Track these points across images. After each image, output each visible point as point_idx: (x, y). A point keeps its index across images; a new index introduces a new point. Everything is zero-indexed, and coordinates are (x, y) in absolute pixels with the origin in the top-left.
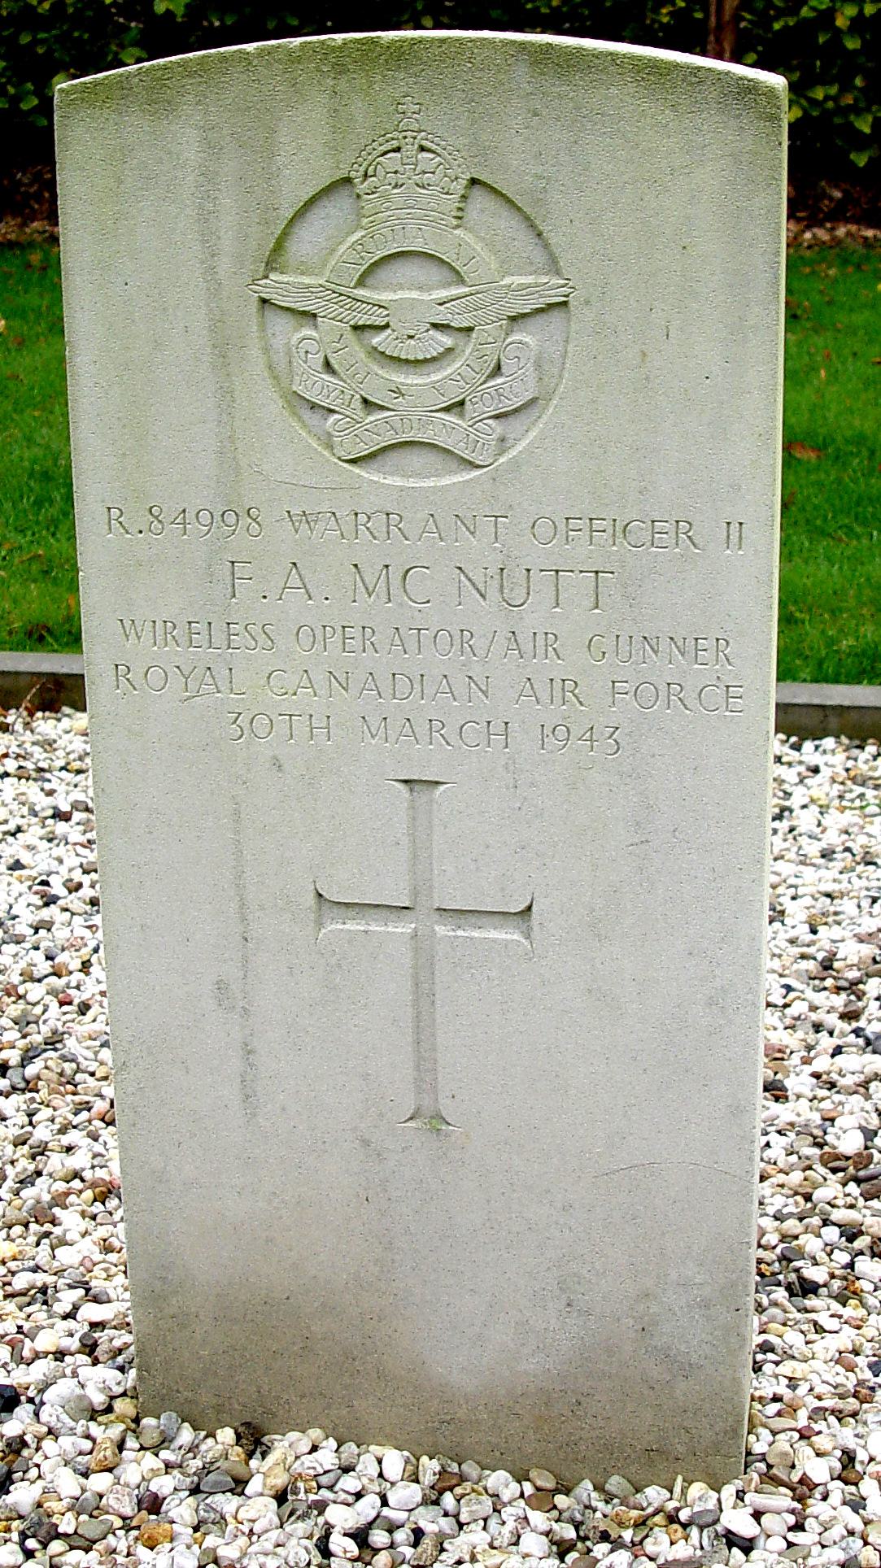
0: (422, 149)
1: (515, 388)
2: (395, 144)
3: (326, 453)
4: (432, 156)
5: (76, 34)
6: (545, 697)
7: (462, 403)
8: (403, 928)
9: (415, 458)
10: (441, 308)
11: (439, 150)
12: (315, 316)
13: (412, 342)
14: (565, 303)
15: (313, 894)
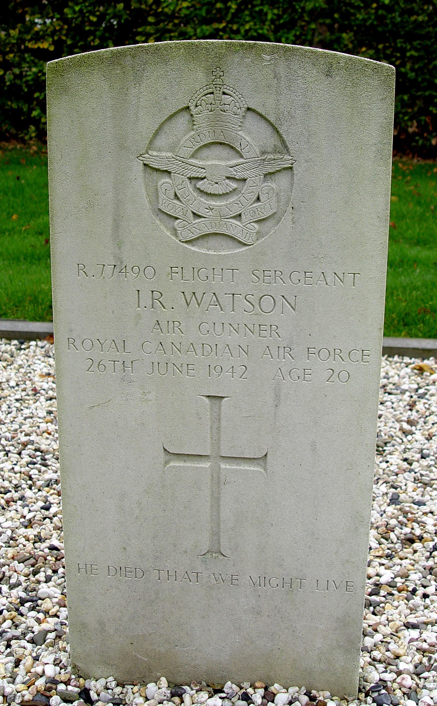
0: (224, 93)
1: (266, 208)
2: (211, 90)
3: (174, 238)
4: (229, 97)
7: (240, 215)
8: (206, 465)
13: (217, 185)
14: (291, 168)
15: (162, 449)
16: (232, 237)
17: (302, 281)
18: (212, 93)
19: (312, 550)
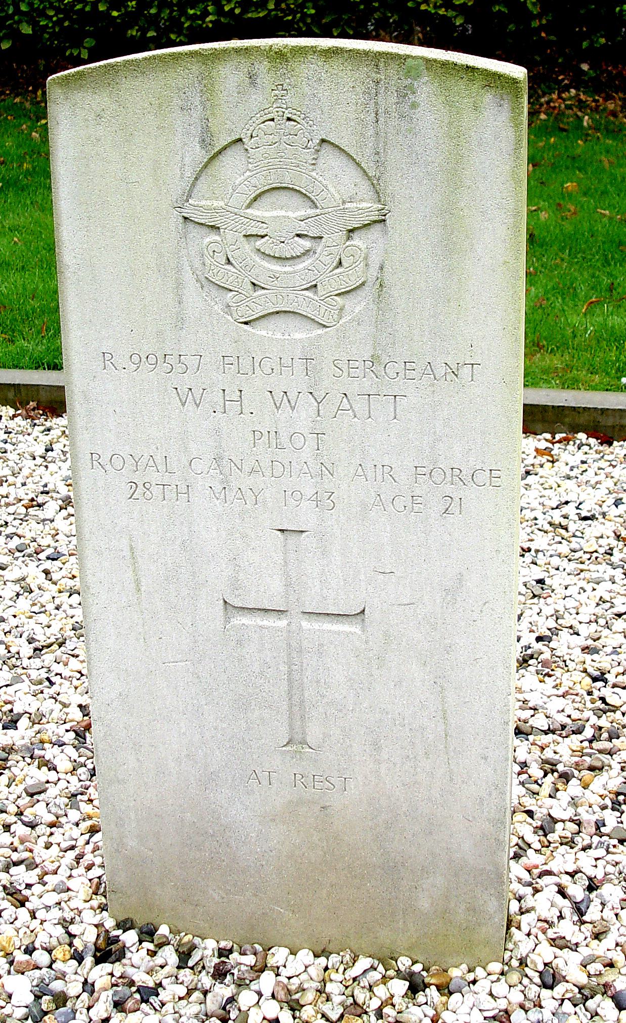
0: (289, 119)
2: (270, 116)
5: (78, 7)
6: (370, 474)
7: (315, 286)
8: (282, 623)
9: (72, 335)
10: (302, 223)
11: (298, 119)
12: (218, 228)
14: (384, 221)
15: (222, 601)
16: (293, 312)
17: (401, 375)
18: (273, 120)
19: (471, 623)
